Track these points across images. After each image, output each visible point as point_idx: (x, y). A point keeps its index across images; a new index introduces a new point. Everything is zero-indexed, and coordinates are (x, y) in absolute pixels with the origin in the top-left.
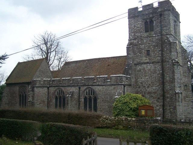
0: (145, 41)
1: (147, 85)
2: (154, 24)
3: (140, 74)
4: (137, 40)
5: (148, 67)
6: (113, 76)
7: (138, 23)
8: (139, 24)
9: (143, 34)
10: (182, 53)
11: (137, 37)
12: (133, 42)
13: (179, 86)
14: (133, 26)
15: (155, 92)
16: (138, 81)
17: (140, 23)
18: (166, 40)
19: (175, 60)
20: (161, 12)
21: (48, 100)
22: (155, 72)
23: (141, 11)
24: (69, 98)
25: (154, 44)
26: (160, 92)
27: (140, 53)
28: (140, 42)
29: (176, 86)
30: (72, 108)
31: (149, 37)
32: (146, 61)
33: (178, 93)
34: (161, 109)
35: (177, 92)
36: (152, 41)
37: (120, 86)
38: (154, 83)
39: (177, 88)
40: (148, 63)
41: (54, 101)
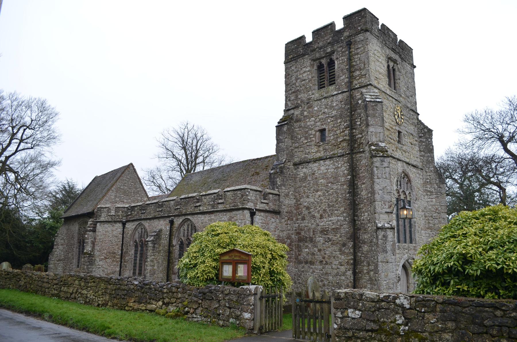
0: (316, 109)
1: (319, 212)
2: (336, 67)
3: (305, 187)
4: (300, 109)
5: (322, 168)
6: (229, 189)
7: (304, 69)
8: (305, 72)
9: (313, 94)
10: (421, 137)
11: (302, 101)
12: (293, 114)
13: (388, 210)
14: (293, 79)
15: (337, 228)
16: (301, 204)
17: (307, 70)
18: (359, 99)
19: (377, 145)
20: (349, 36)
21: (122, 250)
22: (336, 177)
23: (311, 43)
24: (150, 244)
25: (334, 113)
26: (346, 228)
27: (306, 138)
28: (305, 113)
29: (378, 209)
30: (156, 267)
31: (325, 98)
32: (319, 155)
33: (382, 228)
34: (350, 273)
35: (380, 225)
36: (332, 107)
37: (241, 212)
38: (333, 206)
39: (381, 216)
40: (321, 159)
41: (132, 252)
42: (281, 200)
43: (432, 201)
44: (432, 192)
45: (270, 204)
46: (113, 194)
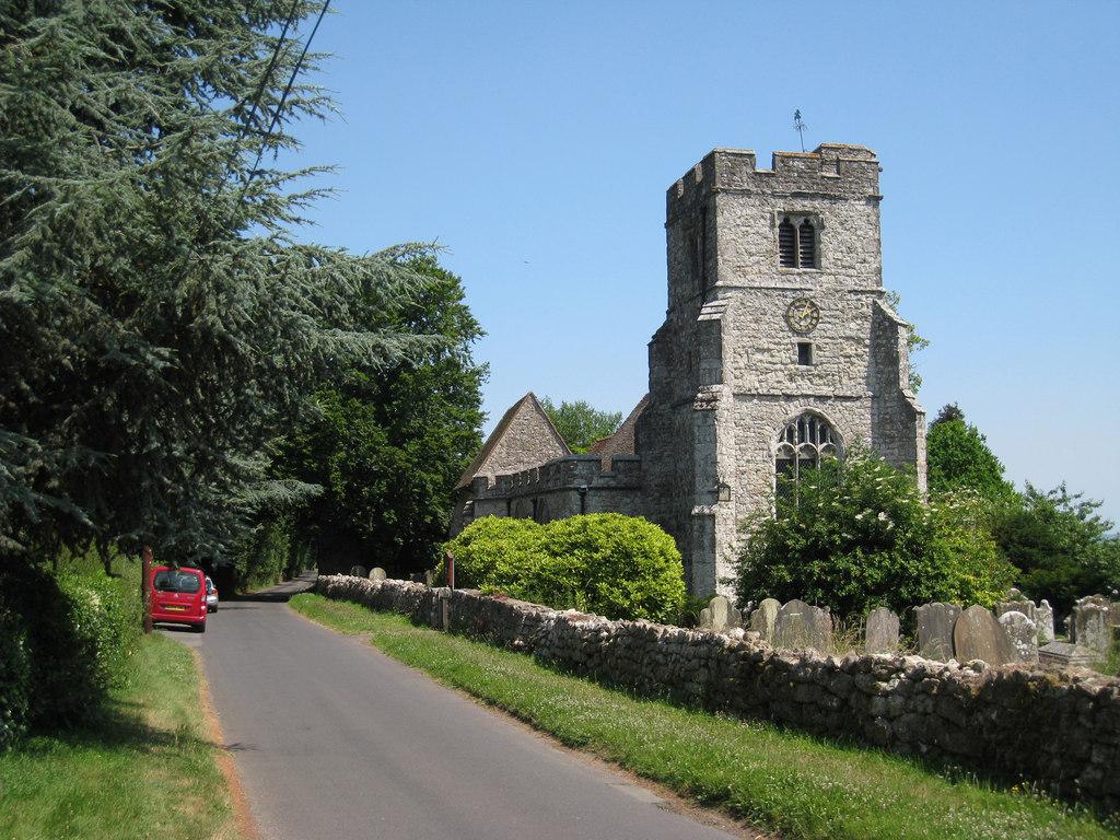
42: (644, 467)
43: (892, 454)
44: (893, 437)
45: (619, 476)
46: (504, 451)
